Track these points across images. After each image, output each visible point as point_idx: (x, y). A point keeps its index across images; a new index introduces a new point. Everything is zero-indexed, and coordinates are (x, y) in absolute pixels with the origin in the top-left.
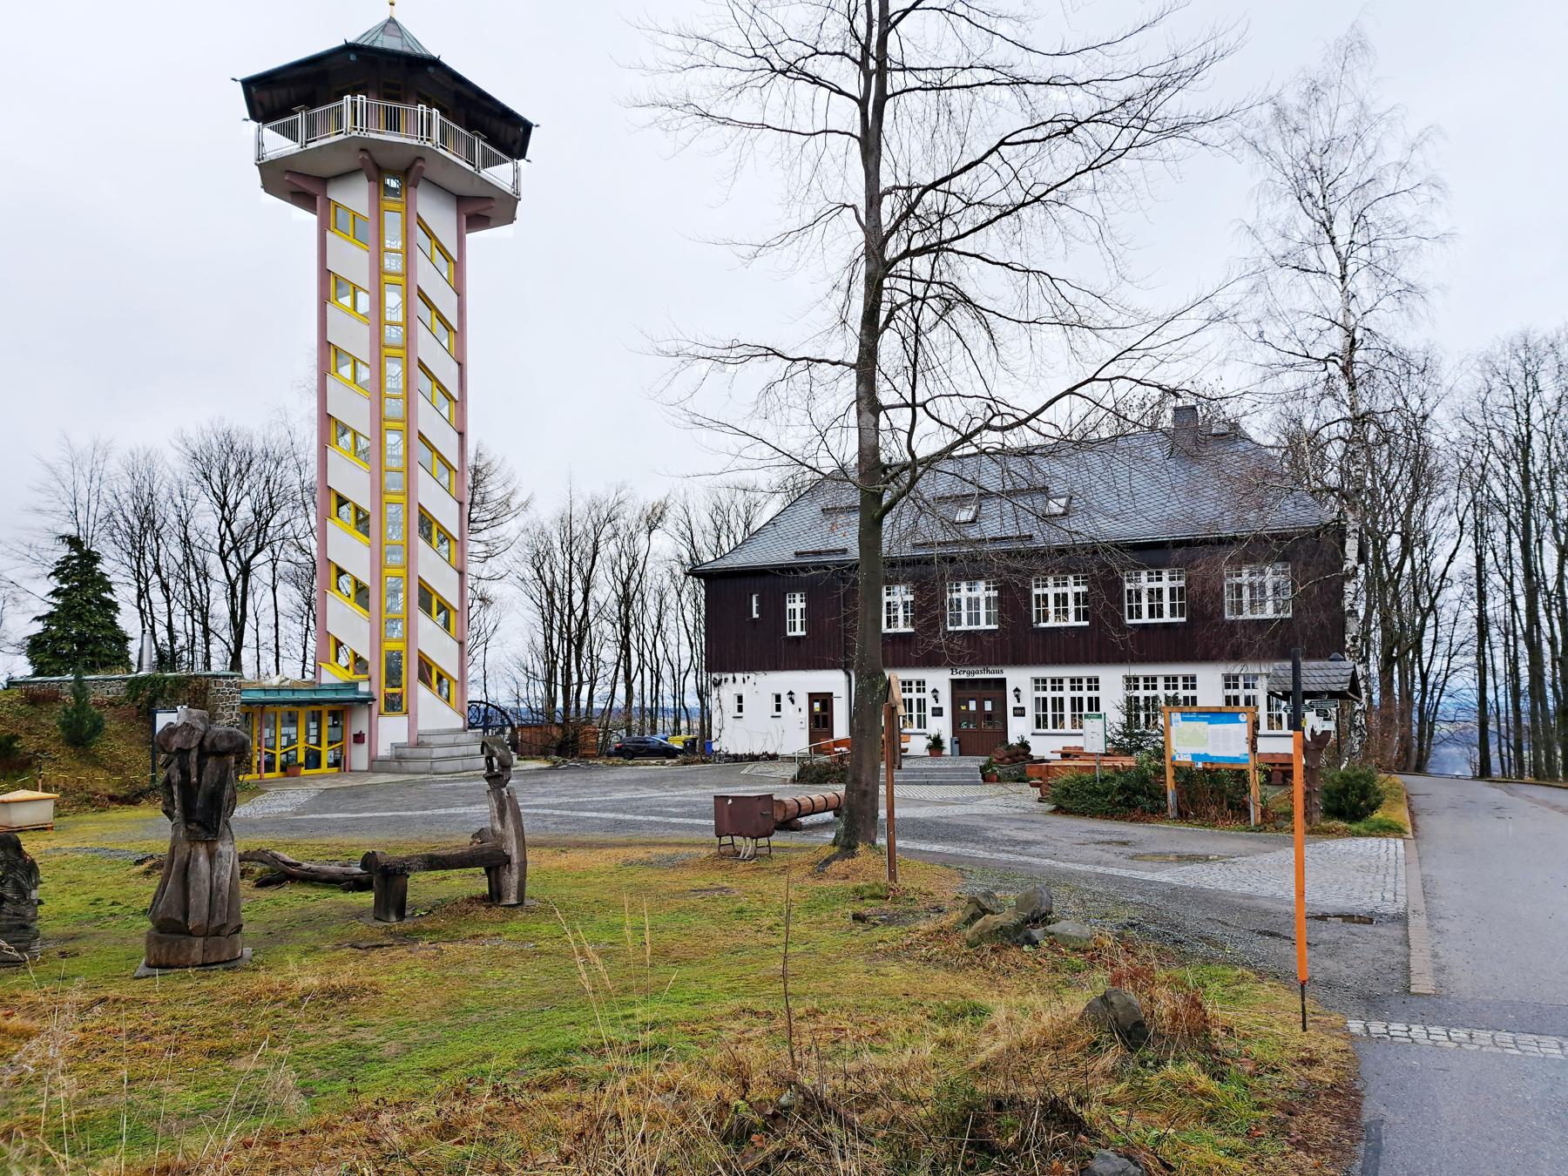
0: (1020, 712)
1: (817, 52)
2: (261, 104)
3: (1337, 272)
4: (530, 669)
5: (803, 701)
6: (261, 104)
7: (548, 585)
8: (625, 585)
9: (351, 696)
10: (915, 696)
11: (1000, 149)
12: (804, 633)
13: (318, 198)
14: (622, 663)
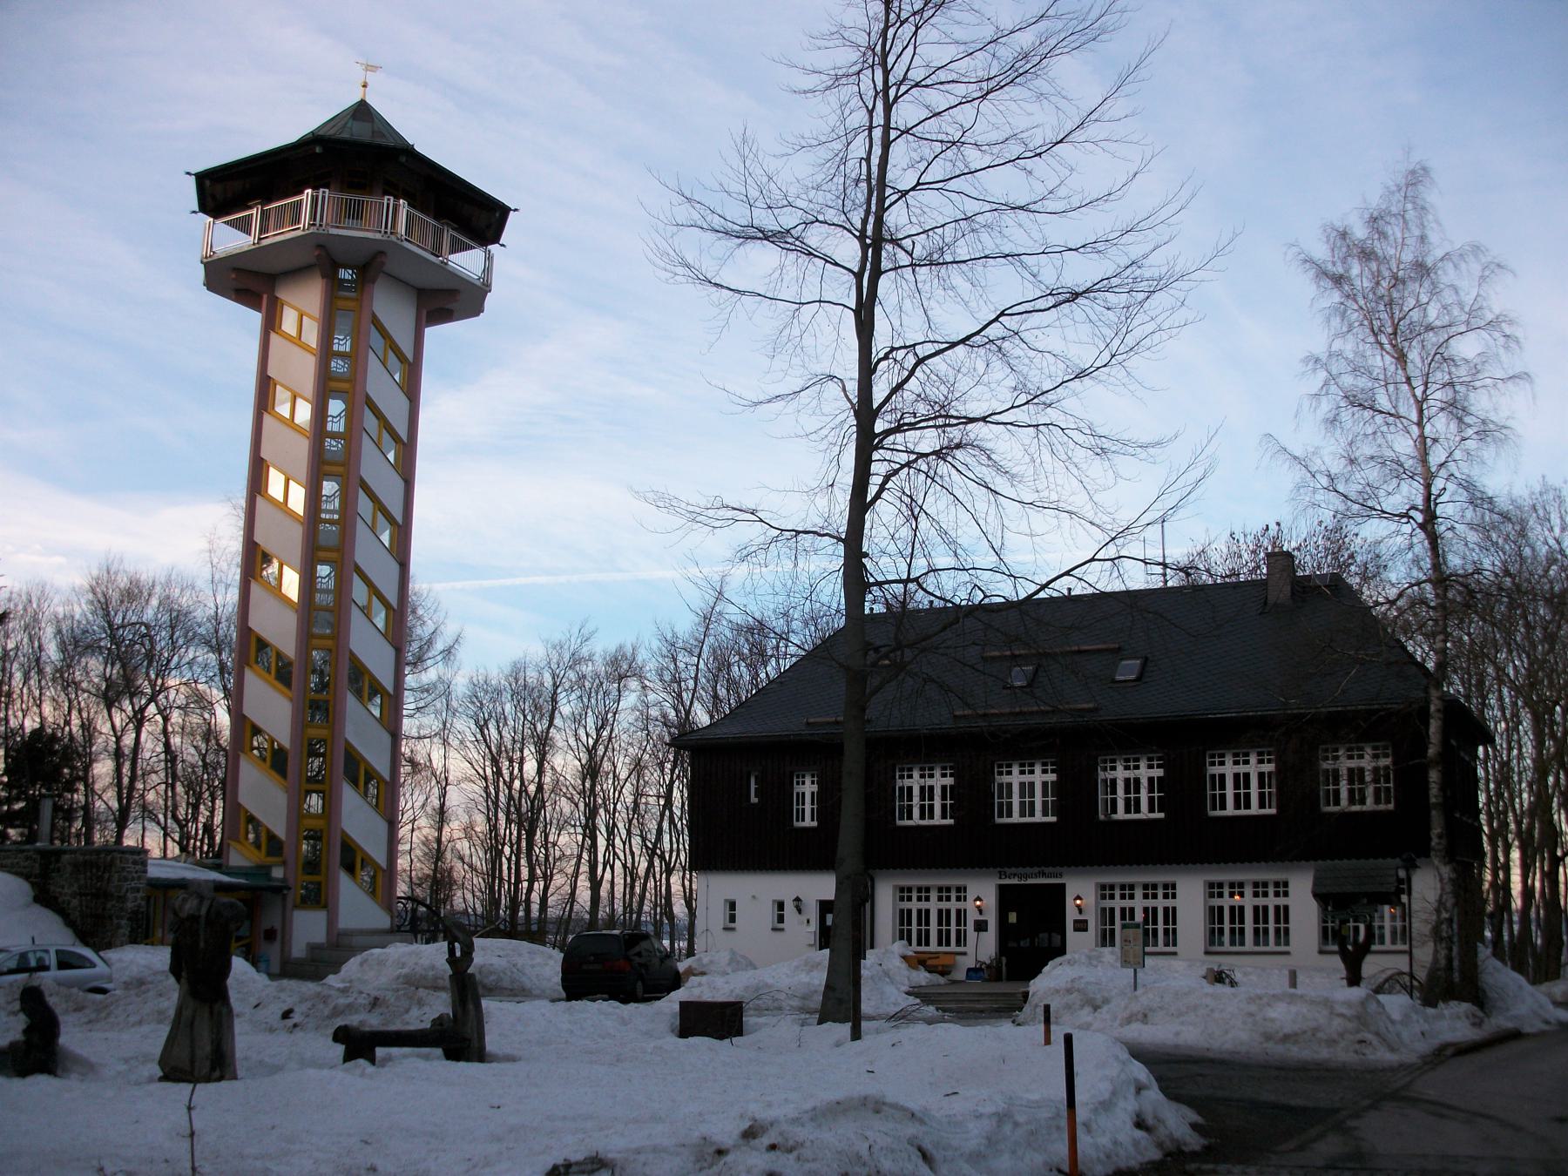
0: (1081, 926)
1: (817, 221)
3: (1414, 417)
4: (467, 860)
5: (813, 913)
6: (213, 197)
8: (591, 751)
9: (262, 883)
10: (953, 905)
11: (1000, 319)
12: (815, 824)
13: (265, 296)
14: (585, 855)
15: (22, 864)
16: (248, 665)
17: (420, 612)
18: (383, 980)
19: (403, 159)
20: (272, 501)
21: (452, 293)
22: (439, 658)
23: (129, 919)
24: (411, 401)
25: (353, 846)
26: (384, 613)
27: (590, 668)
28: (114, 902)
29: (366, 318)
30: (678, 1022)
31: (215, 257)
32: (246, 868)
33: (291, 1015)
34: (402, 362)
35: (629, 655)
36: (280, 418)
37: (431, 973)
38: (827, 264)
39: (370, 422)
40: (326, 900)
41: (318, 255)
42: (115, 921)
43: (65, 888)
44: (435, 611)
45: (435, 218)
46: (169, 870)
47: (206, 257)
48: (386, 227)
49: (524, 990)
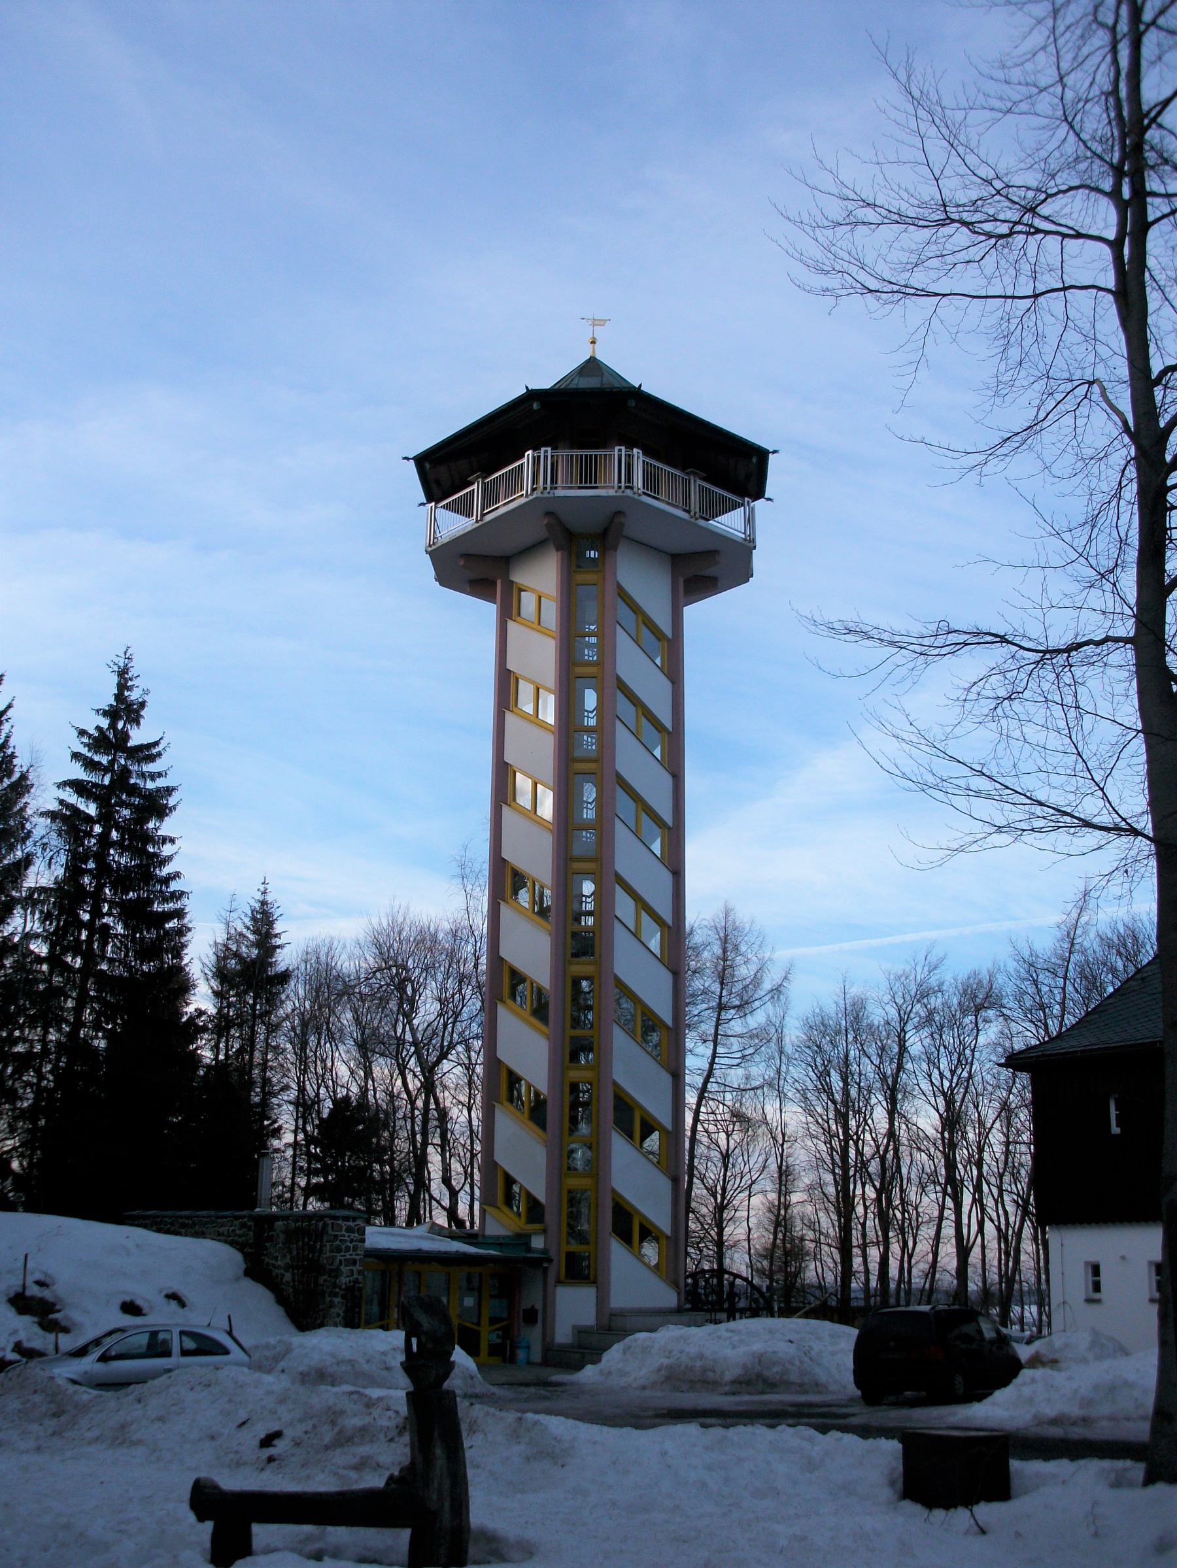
2: (438, 482)
6: (438, 482)
7: (838, 1097)
8: (949, 1102)
13: (499, 582)
15: (238, 1232)
16: (502, 1000)
17: (743, 948)
18: (644, 1372)
19: (632, 403)
20: (521, 810)
21: (710, 555)
22: (767, 998)
23: (343, 1297)
24: (673, 683)
25: (629, 1209)
26: (658, 935)
27: (939, 1001)
28: (326, 1277)
29: (610, 590)
30: (901, 1468)
31: (439, 544)
32: (504, 1237)
33: (275, 1442)
34: (659, 640)
35: (985, 982)
36: (524, 716)
37: (699, 1364)
38: (1066, 241)
39: (624, 707)
40: (596, 1277)
41: (546, 525)
42: (328, 1299)
43: (279, 1260)
44: (760, 946)
45: (683, 470)
46: (402, 1239)
47: (430, 546)
48: (620, 481)
49: (817, 1385)
